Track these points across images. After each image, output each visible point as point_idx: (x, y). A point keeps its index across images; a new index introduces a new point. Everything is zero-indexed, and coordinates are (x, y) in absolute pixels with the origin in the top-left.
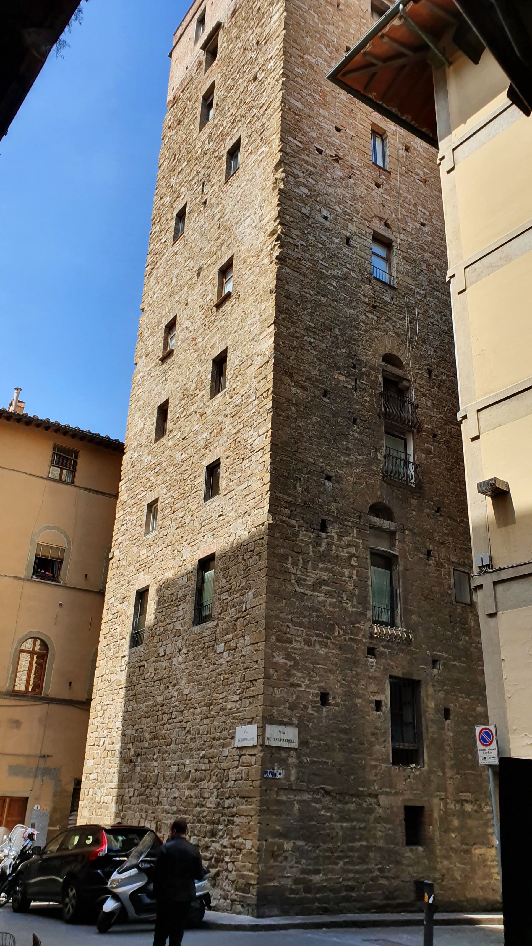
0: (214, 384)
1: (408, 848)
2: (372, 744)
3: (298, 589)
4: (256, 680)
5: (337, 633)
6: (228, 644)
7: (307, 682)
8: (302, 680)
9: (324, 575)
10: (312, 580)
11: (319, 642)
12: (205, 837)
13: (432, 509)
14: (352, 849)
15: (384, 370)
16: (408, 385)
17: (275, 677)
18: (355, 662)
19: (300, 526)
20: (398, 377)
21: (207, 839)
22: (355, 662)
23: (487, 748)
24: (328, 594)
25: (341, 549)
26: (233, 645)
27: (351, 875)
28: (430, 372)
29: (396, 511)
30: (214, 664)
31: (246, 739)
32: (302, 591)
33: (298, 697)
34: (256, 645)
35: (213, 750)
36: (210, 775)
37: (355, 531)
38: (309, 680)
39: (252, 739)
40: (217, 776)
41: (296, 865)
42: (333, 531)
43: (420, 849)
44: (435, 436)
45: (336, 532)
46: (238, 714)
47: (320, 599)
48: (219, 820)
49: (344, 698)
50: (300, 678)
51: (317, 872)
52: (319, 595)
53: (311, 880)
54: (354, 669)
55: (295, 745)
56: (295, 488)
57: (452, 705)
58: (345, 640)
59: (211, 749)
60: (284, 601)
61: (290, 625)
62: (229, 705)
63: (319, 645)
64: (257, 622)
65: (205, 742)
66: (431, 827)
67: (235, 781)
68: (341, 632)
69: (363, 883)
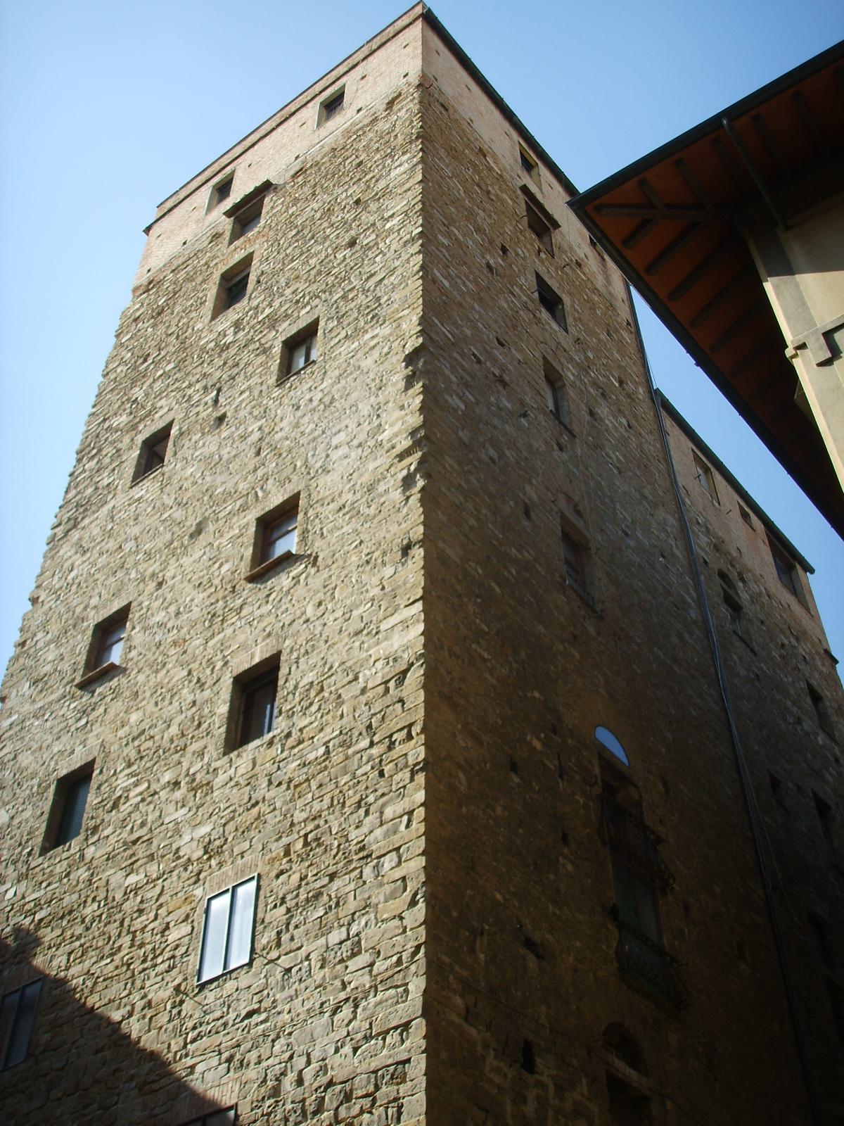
28: (665, 783)
37: (584, 1081)
42: (546, 1069)
44: (687, 908)
56: (472, 950)
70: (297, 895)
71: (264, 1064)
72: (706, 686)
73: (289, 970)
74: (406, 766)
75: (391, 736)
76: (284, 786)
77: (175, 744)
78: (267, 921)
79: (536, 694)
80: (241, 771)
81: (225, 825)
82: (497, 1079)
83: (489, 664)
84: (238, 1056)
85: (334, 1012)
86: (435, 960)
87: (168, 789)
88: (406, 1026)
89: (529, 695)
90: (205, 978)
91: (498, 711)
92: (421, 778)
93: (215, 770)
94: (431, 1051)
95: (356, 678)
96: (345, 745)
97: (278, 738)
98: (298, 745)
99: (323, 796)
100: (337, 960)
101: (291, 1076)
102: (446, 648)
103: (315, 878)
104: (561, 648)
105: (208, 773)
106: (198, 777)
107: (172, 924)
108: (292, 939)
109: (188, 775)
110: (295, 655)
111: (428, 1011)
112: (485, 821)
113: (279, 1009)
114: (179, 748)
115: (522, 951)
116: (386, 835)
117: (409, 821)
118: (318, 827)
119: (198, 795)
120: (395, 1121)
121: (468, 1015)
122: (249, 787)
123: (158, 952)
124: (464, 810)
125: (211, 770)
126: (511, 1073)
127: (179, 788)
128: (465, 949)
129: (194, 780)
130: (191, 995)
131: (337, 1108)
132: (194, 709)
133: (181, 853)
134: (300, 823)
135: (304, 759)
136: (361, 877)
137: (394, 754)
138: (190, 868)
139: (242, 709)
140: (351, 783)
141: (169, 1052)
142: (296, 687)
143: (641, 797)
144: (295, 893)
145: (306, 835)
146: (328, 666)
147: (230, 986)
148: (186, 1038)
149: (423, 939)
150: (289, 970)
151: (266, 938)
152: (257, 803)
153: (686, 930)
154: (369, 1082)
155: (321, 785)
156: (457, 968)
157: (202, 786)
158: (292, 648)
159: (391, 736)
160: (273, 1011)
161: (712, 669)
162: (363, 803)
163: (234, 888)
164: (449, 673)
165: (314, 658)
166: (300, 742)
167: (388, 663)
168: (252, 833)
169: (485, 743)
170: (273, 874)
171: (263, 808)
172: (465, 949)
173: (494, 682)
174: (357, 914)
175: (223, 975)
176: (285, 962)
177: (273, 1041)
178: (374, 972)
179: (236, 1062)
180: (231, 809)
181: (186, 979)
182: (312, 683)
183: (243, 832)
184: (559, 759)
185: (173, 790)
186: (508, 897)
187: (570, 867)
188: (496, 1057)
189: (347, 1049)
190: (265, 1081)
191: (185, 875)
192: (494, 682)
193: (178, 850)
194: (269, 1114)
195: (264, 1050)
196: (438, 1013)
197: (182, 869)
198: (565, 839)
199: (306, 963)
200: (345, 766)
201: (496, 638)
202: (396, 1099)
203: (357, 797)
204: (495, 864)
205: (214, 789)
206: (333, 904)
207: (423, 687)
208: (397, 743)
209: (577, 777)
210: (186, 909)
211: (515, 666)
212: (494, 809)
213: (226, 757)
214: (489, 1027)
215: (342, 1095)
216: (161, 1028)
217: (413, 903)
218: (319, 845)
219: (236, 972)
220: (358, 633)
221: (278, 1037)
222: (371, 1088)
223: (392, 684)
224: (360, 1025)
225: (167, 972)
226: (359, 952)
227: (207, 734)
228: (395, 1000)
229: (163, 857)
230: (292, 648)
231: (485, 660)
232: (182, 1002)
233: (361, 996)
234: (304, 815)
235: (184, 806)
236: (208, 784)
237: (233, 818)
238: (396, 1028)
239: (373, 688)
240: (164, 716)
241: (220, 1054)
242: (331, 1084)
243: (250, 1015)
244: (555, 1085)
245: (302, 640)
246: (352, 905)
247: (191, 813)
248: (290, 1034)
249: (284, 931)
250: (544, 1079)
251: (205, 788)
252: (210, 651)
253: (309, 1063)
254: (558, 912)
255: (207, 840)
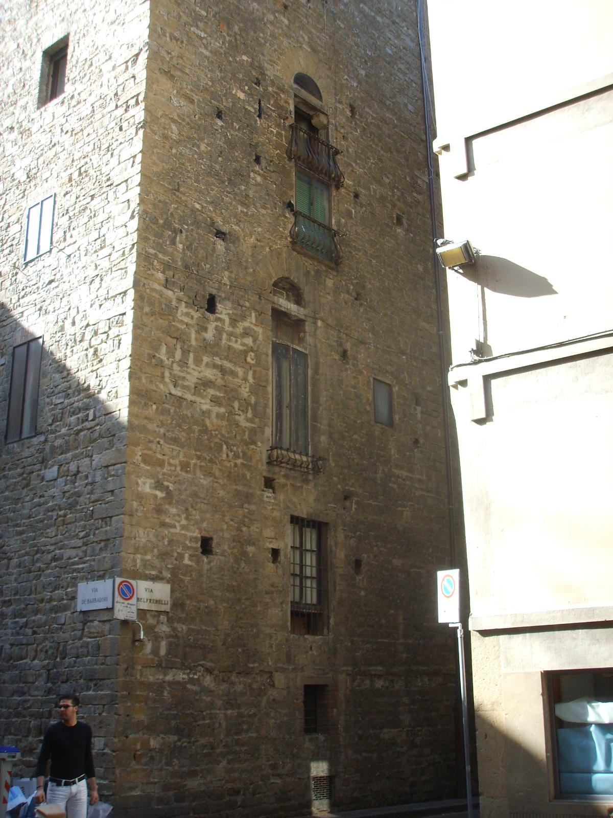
0: (44, 88)
1: (307, 738)
2: (266, 606)
3: (174, 392)
4: (111, 517)
5: (224, 456)
6: (64, 468)
7: (184, 522)
8: (177, 518)
9: (210, 374)
10: (194, 380)
11: (201, 467)
12: (27, 736)
13: (351, 294)
14: (237, 742)
15: (296, 96)
16: (325, 122)
17: (140, 514)
18: (248, 498)
19: (179, 300)
20: (314, 108)
21: (30, 739)
22: (248, 498)
23: (126, 602)
24: (215, 401)
25: (234, 339)
26: (73, 467)
27: (236, 775)
28: (353, 110)
29: (307, 292)
30: (41, 497)
31: (95, 600)
32: (179, 394)
33: (171, 542)
34: (111, 468)
35: (39, 616)
36: (36, 651)
37: (253, 315)
38: (187, 518)
39: (105, 599)
40: (47, 652)
41: (165, 768)
42: (224, 310)
43: (321, 737)
44: (356, 196)
45: (229, 314)
46: (81, 566)
47: (205, 407)
48: (50, 712)
49: (232, 545)
50: (174, 515)
51: (193, 774)
52: (203, 401)
53: (185, 785)
54: (246, 505)
55: (167, 608)
56: (173, 242)
57: (366, 556)
58: (236, 465)
59: (36, 614)
60: (154, 407)
61: (162, 442)
62: (69, 553)
63: (201, 471)
64: (114, 435)
65: (27, 605)
66: (335, 710)
67: (77, 657)
68: (231, 455)
69: (251, 784)
70: (75, 208)
71: (57, 312)
72: (405, 29)
73: (69, 256)
74: (134, 124)
75: (127, 102)
76: (69, 134)
77: (11, 100)
78: (59, 224)
79: (245, 58)
80: (47, 121)
81: (38, 159)
82: (186, 320)
83: (204, 41)
84: (44, 308)
85: (91, 283)
86: (144, 253)
87: (8, 132)
88: (125, 293)
89: (238, 59)
90: (28, 260)
91: (209, 76)
92: (141, 132)
93: (32, 120)
94: (137, 308)
95: (110, 58)
96: (103, 106)
97: (67, 98)
98: (77, 104)
99: (89, 142)
100: (93, 251)
101: (70, 321)
102: (168, 35)
103: (84, 197)
104: (272, 18)
105: (29, 122)
106: (24, 124)
107: (11, 224)
108: (71, 236)
109: (18, 122)
110: (77, 38)
111: (136, 285)
112: (191, 156)
113: (64, 280)
114: (13, 103)
115: (213, 239)
116: (121, 172)
117: (134, 162)
118: (87, 163)
119: (24, 137)
120: (117, 348)
121: (167, 284)
122: (50, 133)
123: (4, 242)
124: (174, 151)
125: (30, 120)
126: (196, 315)
127: (14, 132)
128: (168, 243)
129: (21, 126)
130: (21, 269)
131: (90, 340)
132: (21, 74)
133: (15, 177)
134: (77, 160)
135: (80, 115)
136: (107, 199)
137: (128, 115)
138: (20, 187)
139: (51, 73)
140: (104, 134)
141: (11, 303)
142: (77, 62)
143: (328, 122)
144: (74, 206)
145: (80, 168)
146: (95, 47)
147: (40, 264)
148: (19, 295)
149: (135, 241)
150: (69, 256)
151: (58, 235)
152: (55, 144)
153: (353, 211)
154: (106, 325)
155: (89, 135)
156: (161, 256)
157: (25, 131)
158: (76, 31)
159: (127, 102)
160: (61, 281)
161: (415, 13)
162: (110, 148)
163: (42, 201)
164: (169, 53)
165: (88, 40)
166: (79, 103)
167: (128, 47)
168: (52, 165)
169: (196, 101)
170: (62, 194)
171: (58, 148)
172: (168, 243)
173: (208, 54)
174: (105, 222)
175: (37, 258)
176: (68, 251)
177: (61, 299)
178: (111, 260)
179: (43, 311)
180: (41, 148)
181: (18, 259)
182: (86, 59)
183: (48, 164)
184: (260, 103)
185: (10, 133)
186: (205, 205)
187: (259, 179)
188: (186, 307)
189: (96, 306)
190: (57, 322)
191: (17, 192)
192: (208, 54)
193: (13, 174)
194: (59, 341)
195: (57, 304)
196: (144, 284)
197: (15, 188)
198: (258, 160)
199: (78, 252)
200: (102, 122)
201: (213, 19)
202: (118, 336)
203: (107, 145)
204: (196, 184)
205: (33, 133)
206: (92, 215)
207: (146, 68)
208: (130, 107)
209: (274, 114)
210: (18, 214)
211: (227, 38)
212: (199, 147)
213: (39, 111)
214: (182, 289)
215: (93, 332)
216: (7, 288)
217: (132, 217)
218: (86, 176)
219: (43, 256)
220: (113, 23)
221: (64, 297)
222: (107, 329)
223: (130, 64)
224: (103, 293)
225: (9, 254)
226: (105, 247)
227: (29, 93)
228: (120, 277)
229: (5, 179)
230: (76, 31)
231: (201, 38)
232: (17, 273)
233: (104, 274)
234: (80, 154)
235: (16, 144)
236: (29, 129)
237: (42, 155)
238: (120, 294)
239: (120, 66)
240: (4, 78)
241: (36, 305)
242: (88, 325)
243: (51, 282)
244: (230, 318)
245: (81, 27)
246: (101, 217)
247: (21, 149)
248: (69, 295)
249: (68, 231)
250: (223, 316)
251: (27, 133)
252: (29, 30)
253: (78, 312)
254: (245, 210)
255: (28, 169)
